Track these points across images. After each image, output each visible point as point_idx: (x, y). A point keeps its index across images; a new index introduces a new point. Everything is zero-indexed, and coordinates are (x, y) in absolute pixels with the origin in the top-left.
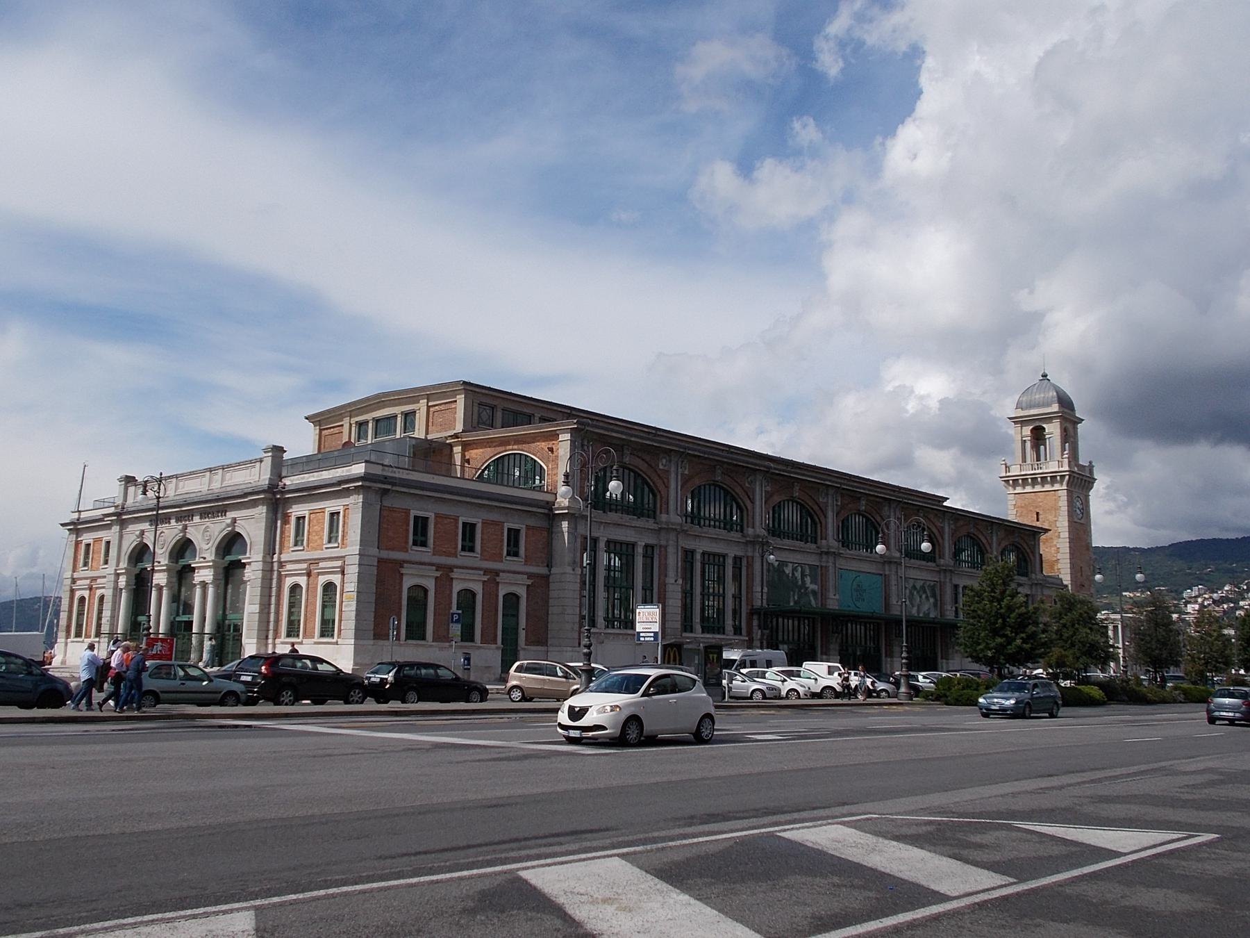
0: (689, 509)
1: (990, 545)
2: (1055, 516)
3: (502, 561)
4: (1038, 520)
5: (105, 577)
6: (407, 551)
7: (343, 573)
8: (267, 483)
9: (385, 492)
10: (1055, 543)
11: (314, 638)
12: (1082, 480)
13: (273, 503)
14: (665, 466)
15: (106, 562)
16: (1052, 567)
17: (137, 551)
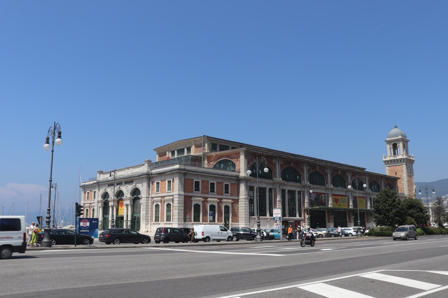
0: (254, 172)
1: (381, 184)
2: (402, 173)
3: (223, 195)
4: (396, 175)
5: (94, 203)
6: (193, 193)
7: (173, 200)
8: (146, 172)
9: (185, 174)
10: (402, 182)
11: (164, 222)
12: (410, 161)
13: (148, 178)
14: (275, 162)
15: (94, 198)
16: (401, 190)
17: (104, 194)
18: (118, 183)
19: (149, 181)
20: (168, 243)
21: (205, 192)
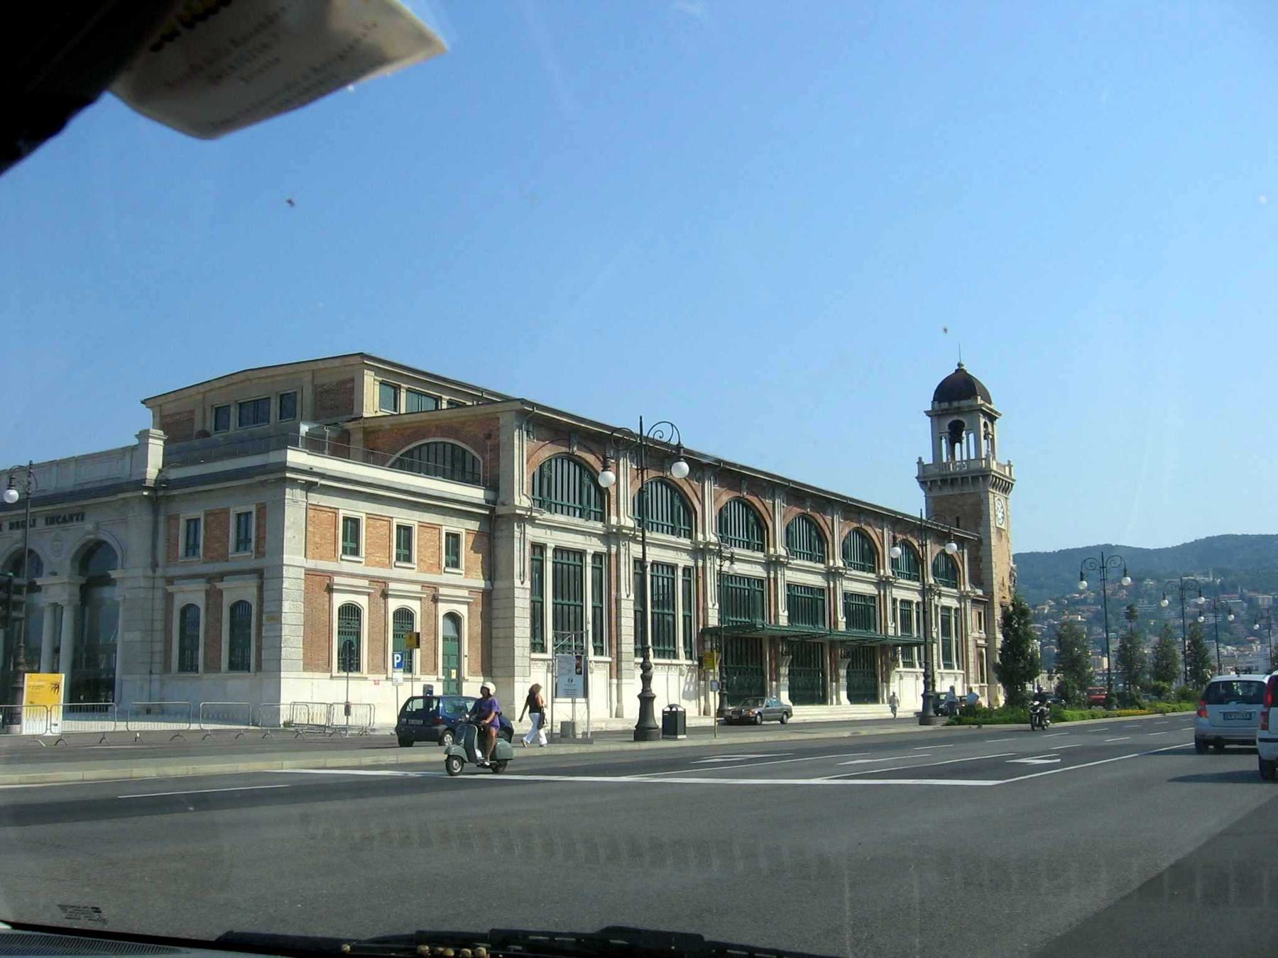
18: (18, 523)
19: (156, 512)
20: (411, 746)
21: (378, 559)
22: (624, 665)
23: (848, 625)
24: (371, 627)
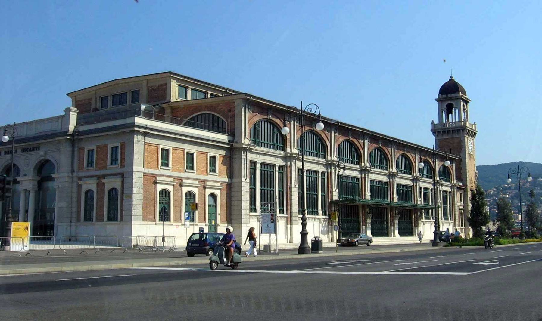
18: (8, 151)
19: (73, 146)
21: (178, 168)
22: (293, 218)
23: (399, 199)
24: (175, 200)
